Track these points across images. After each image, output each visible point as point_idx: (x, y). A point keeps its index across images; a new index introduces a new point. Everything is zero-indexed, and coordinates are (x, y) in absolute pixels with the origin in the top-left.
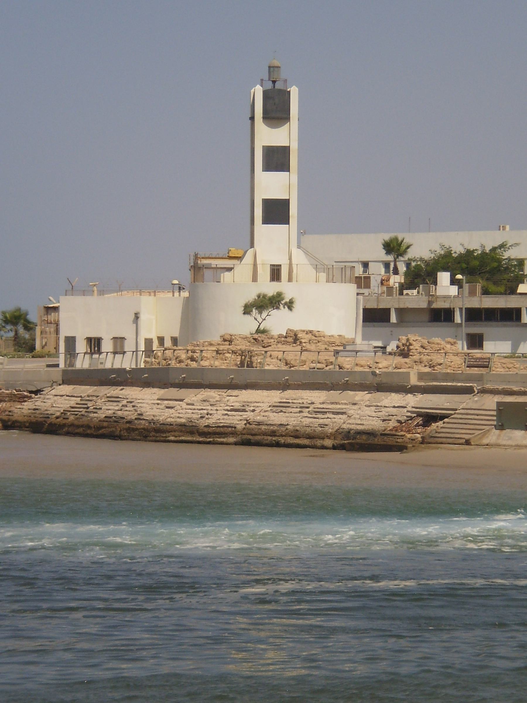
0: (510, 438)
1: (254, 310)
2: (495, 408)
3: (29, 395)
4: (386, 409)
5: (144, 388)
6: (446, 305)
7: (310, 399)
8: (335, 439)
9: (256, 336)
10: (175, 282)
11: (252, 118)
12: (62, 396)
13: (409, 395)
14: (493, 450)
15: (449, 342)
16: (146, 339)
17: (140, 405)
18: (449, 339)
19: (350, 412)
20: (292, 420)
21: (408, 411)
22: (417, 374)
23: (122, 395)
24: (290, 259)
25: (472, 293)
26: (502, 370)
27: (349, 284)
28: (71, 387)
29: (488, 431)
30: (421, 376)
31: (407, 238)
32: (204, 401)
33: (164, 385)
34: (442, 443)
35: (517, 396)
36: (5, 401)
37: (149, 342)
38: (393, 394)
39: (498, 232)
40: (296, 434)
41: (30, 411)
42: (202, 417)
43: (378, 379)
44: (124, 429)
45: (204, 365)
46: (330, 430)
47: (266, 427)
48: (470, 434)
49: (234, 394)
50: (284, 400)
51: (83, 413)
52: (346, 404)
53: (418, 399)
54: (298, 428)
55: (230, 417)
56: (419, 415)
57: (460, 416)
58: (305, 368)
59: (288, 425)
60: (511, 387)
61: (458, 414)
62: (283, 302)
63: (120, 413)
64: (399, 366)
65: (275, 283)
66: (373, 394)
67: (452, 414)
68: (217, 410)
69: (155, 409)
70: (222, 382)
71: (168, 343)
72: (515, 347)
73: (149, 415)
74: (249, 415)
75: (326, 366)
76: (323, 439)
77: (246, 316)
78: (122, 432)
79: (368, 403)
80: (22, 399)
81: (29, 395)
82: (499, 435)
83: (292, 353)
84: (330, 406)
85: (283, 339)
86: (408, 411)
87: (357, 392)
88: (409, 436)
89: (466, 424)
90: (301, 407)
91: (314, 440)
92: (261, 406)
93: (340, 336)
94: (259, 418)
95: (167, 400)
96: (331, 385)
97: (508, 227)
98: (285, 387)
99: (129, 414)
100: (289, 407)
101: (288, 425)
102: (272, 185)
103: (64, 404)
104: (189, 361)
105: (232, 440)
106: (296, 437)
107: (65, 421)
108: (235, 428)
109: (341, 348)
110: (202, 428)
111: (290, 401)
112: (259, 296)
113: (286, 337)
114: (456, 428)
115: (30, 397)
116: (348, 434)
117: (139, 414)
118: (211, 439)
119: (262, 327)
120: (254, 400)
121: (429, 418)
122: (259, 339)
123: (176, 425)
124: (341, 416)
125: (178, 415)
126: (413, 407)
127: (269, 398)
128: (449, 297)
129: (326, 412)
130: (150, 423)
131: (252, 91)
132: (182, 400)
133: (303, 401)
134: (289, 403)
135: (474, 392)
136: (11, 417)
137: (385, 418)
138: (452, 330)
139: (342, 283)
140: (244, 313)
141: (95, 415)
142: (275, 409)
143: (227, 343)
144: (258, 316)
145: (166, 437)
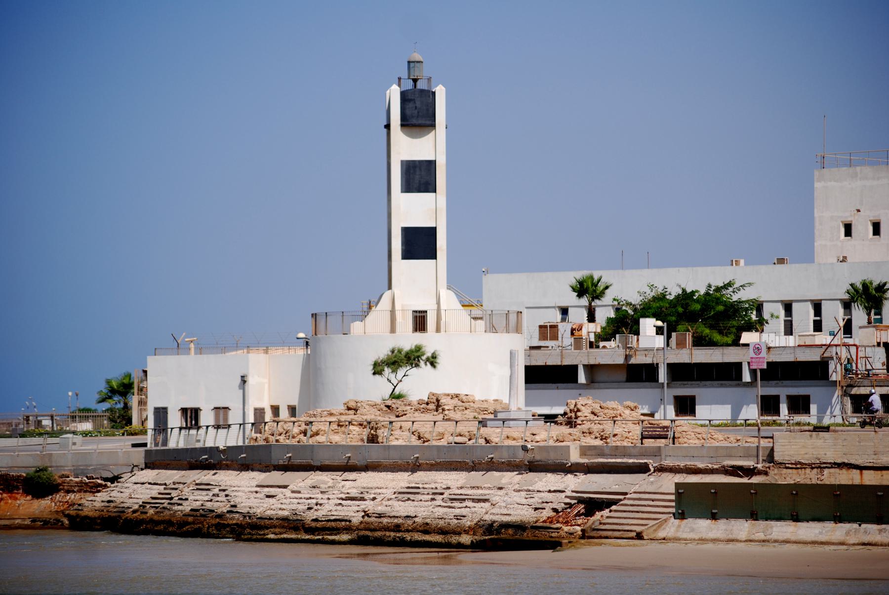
0: (692, 530)
1: (386, 369)
2: (673, 491)
3: (104, 483)
4: (539, 494)
5: (241, 471)
6: (648, 360)
7: (445, 482)
8: (474, 534)
9: (389, 403)
10: (302, 335)
11: (388, 127)
12: (143, 484)
13: (569, 475)
14: (670, 545)
15: (628, 407)
16: (256, 409)
17: (235, 493)
18: (628, 403)
19: (494, 499)
20: (423, 510)
21: (566, 497)
22: (578, 449)
23: (214, 480)
24: (438, 303)
25: (681, 344)
26: (697, 441)
27: (506, 335)
28: (156, 471)
29: (666, 520)
30: (585, 451)
31: (606, 276)
32: (314, 487)
33: (266, 468)
34: (607, 538)
35: (703, 476)
36: (73, 492)
37: (259, 413)
38: (549, 475)
39: (730, 267)
40: (426, 529)
41: (103, 504)
42: (310, 509)
43: (529, 456)
44: (213, 525)
45: (321, 441)
46: (469, 523)
47: (389, 520)
48: (642, 525)
49: (351, 478)
50: (413, 485)
51: (165, 505)
52: (489, 488)
53: (580, 481)
54: (428, 521)
55: (345, 508)
56: (580, 501)
57: (631, 502)
58: (443, 442)
59: (416, 516)
60: (696, 463)
61: (629, 499)
62: (424, 358)
63: (209, 505)
64: (561, 438)
65: (418, 334)
66: (525, 475)
67: (621, 500)
68: (329, 499)
69: (252, 499)
70: (336, 462)
71: (284, 414)
72: (736, 412)
73: (245, 507)
74: (368, 505)
75: (470, 440)
76: (459, 534)
77: (377, 376)
78: (210, 530)
79: (517, 487)
80: (95, 488)
81: (104, 483)
82: (679, 526)
83: (425, 423)
84: (470, 492)
85: (424, 406)
86: (566, 497)
87: (505, 473)
88: (566, 528)
89: (638, 512)
90: (434, 494)
91: (449, 536)
92: (383, 493)
93: (496, 400)
94: (380, 509)
95: (267, 486)
96: (471, 464)
97: (742, 262)
98: (415, 467)
99: (221, 506)
100: (418, 493)
101: (416, 516)
102: (413, 210)
103: (145, 494)
104: (301, 436)
105: (345, 537)
106: (426, 532)
107: (144, 516)
108: (350, 521)
109: (492, 416)
110: (309, 522)
111: (421, 486)
112: (393, 352)
113: (427, 404)
114: (625, 518)
115: (106, 486)
116: (490, 528)
117: (232, 506)
118: (320, 537)
119: (397, 391)
120: (375, 485)
121: (592, 505)
122: (393, 406)
123: (277, 519)
124: (482, 504)
125: (280, 506)
126: (573, 491)
127: (394, 483)
128: (652, 350)
129: (464, 500)
130: (245, 517)
131: (388, 92)
132: (285, 487)
133: (437, 485)
134: (419, 488)
135: (650, 470)
136: (80, 512)
137: (538, 506)
138: (657, 391)
139: (508, 332)
140: (374, 374)
141: (180, 508)
142: (400, 496)
143: (352, 412)
144: (392, 377)
145: (264, 535)
